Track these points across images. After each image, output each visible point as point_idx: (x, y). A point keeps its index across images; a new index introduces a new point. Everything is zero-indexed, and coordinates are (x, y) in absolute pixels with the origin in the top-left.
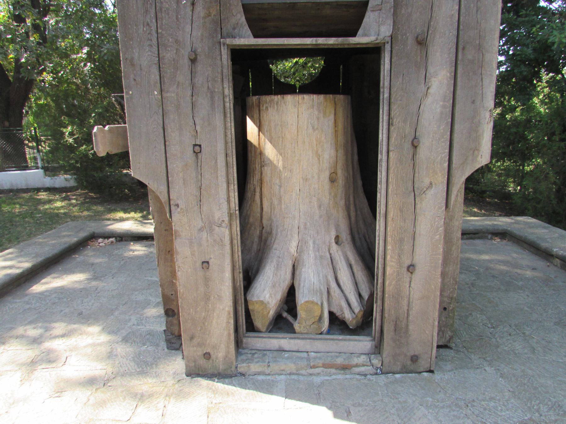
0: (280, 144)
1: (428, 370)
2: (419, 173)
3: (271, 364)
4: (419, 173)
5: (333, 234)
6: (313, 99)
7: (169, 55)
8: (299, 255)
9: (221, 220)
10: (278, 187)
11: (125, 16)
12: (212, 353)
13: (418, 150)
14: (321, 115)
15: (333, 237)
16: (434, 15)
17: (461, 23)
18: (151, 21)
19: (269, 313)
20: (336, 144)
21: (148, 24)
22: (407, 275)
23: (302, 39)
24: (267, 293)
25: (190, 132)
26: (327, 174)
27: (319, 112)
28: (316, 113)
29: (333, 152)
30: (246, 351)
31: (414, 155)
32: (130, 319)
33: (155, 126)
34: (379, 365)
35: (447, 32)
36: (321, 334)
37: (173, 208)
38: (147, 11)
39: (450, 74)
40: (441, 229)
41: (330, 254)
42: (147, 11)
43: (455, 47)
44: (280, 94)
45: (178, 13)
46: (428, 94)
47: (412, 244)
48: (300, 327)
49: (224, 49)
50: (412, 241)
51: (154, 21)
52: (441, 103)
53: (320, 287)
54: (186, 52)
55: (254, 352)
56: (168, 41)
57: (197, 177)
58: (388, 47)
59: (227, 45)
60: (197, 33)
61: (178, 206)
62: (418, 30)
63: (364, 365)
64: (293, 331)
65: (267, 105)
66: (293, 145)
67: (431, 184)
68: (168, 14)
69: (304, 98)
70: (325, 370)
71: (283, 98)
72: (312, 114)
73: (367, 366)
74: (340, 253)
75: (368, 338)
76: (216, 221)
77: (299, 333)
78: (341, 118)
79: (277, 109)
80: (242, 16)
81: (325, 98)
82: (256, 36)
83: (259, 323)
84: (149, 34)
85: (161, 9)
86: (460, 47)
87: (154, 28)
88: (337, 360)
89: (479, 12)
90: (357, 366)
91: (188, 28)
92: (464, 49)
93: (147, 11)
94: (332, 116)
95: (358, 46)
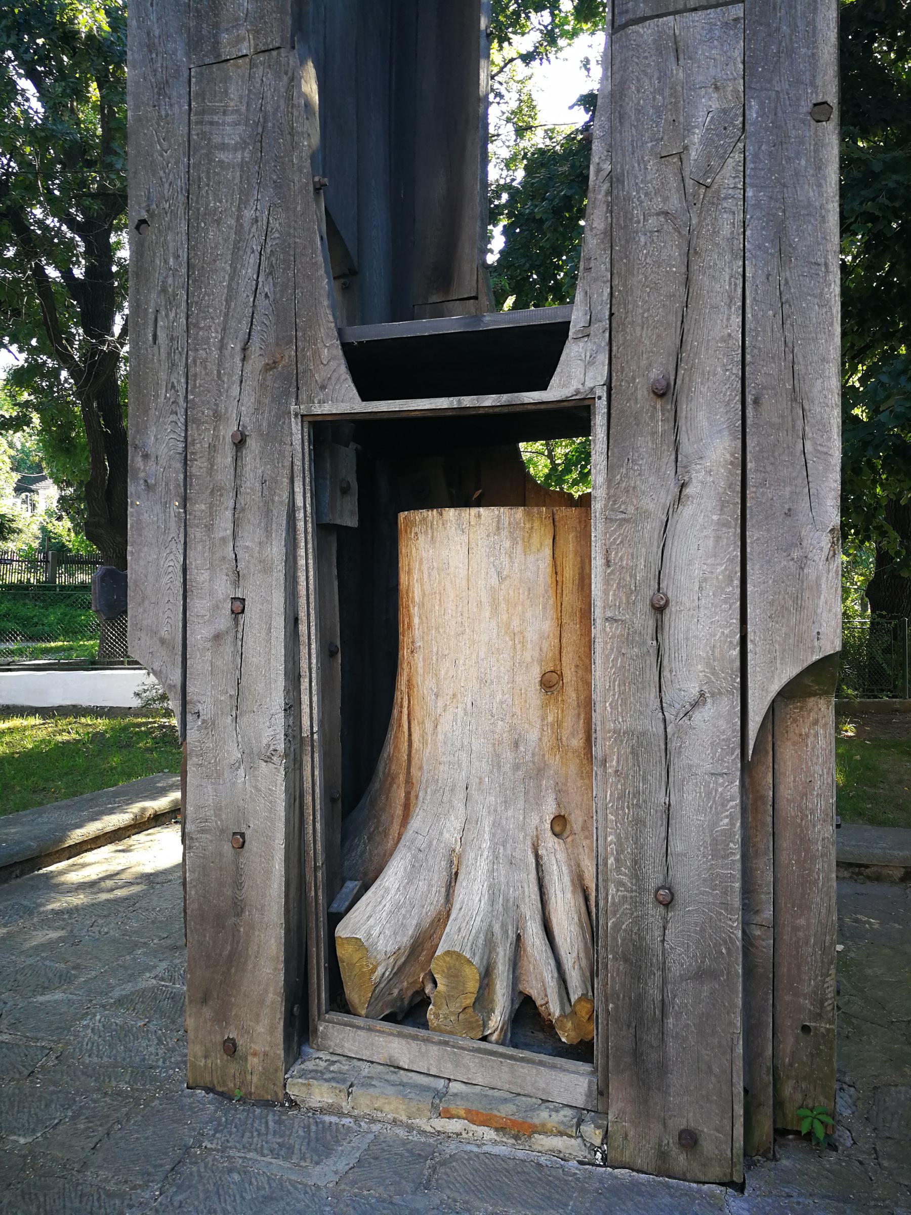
0: (437, 608)
1: (726, 1180)
2: (671, 671)
3: (354, 1089)
4: (671, 671)
5: (550, 809)
6: (499, 517)
7: (203, 437)
8: (463, 851)
9: (272, 748)
10: (433, 697)
11: (139, 375)
12: (240, 1042)
13: (666, 618)
14: (519, 548)
15: (548, 819)
16: (689, 338)
17: (748, 351)
18: (179, 381)
19: (373, 971)
20: (560, 607)
21: (173, 387)
22: (654, 913)
23: (433, 400)
24: (376, 924)
25: (227, 575)
26: (536, 673)
27: (514, 542)
28: (507, 544)
29: (548, 626)
30: (321, 1054)
31: (658, 629)
32: (155, 967)
33: (171, 564)
34: (597, 1141)
35: (719, 369)
36: (484, 1039)
37: (189, 718)
38: (173, 365)
39: (732, 455)
40: (732, 803)
41: (537, 857)
42: (173, 365)
43: (738, 398)
44: (437, 507)
45: (220, 364)
46: (683, 499)
47: (663, 835)
48: (437, 1016)
49: (297, 424)
50: (664, 829)
51: (183, 380)
52: (715, 517)
53: (490, 925)
54: (228, 431)
55: (335, 1058)
56: (203, 413)
57: (233, 662)
58: (601, 406)
59: (302, 416)
60: (249, 401)
61: (199, 716)
62: (655, 373)
63: (561, 1134)
64: (425, 1025)
65: (417, 529)
66: (460, 609)
67: (702, 694)
68: (205, 368)
69: (479, 516)
70: (474, 1127)
71: (441, 515)
72: (497, 547)
73: (570, 1136)
74: (561, 856)
75: (586, 1067)
76: (263, 751)
77: (434, 1030)
78: (571, 556)
79: (432, 537)
80: (339, 365)
81: (528, 514)
82: (364, 399)
83: (355, 994)
84: (173, 403)
85: (195, 362)
86: (749, 399)
87: (182, 393)
88: (501, 1107)
89: (787, 326)
90: (545, 1132)
91: (235, 390)
92: (756, 402)
93: (173, 365)
94: (548, 552)
95: (543, 407)
